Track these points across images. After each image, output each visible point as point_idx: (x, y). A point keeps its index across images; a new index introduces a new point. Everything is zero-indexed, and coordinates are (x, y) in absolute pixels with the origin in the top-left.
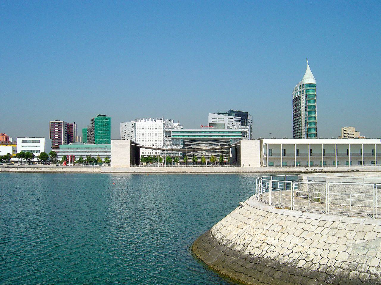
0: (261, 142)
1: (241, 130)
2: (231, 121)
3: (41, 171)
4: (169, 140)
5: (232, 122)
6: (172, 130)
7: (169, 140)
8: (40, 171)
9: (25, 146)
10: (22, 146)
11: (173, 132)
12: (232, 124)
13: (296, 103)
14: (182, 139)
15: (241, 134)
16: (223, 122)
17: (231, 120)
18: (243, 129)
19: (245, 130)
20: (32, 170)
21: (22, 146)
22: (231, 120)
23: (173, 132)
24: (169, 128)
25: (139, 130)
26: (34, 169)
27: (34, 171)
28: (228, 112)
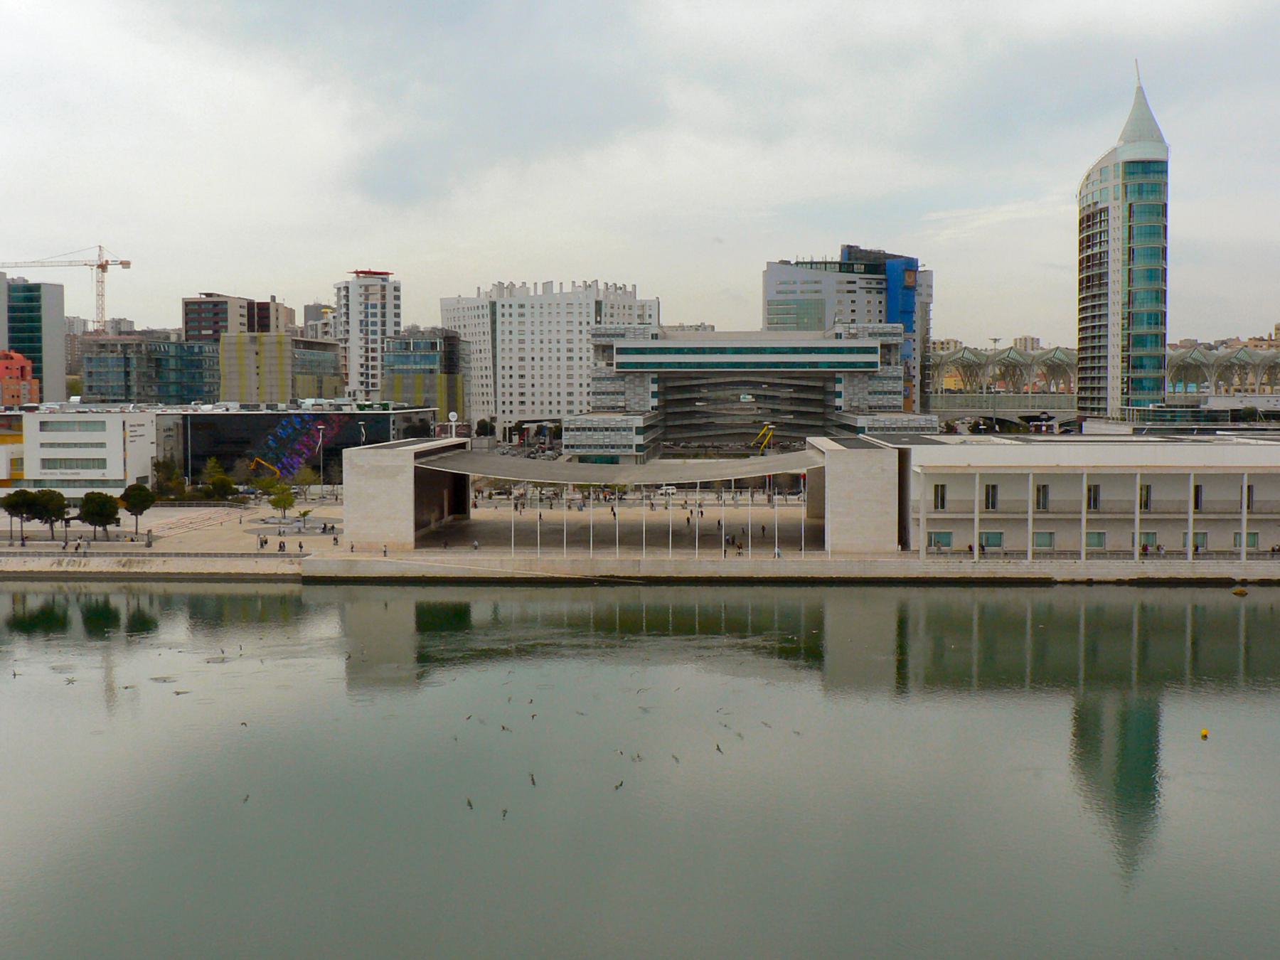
0: (904, 457)
1: (876, 343)
2: (849, 292)
3: (87, 569)
4: (608, 379)
5: (852, 296)
6: (618, 343)
7: (608, 379)
8: (82, 569)
9: (52, 445)
10: (42, 445)
11: (622, 351)
12: (853, 302)
13: (1090, 252)
14: (655, 376)
15: (876, 358)
16: (817, 296)
17: (851, 287)
18: (885, 334)
19: (890, 340)
20: (55, 568)
21: (42, 445)
22: (851, 287)
23: (622, 351)
24: (609, 336)
25: (507, 328)
26: (60, 563)
27: (61, 569)
28: (836, 256)
